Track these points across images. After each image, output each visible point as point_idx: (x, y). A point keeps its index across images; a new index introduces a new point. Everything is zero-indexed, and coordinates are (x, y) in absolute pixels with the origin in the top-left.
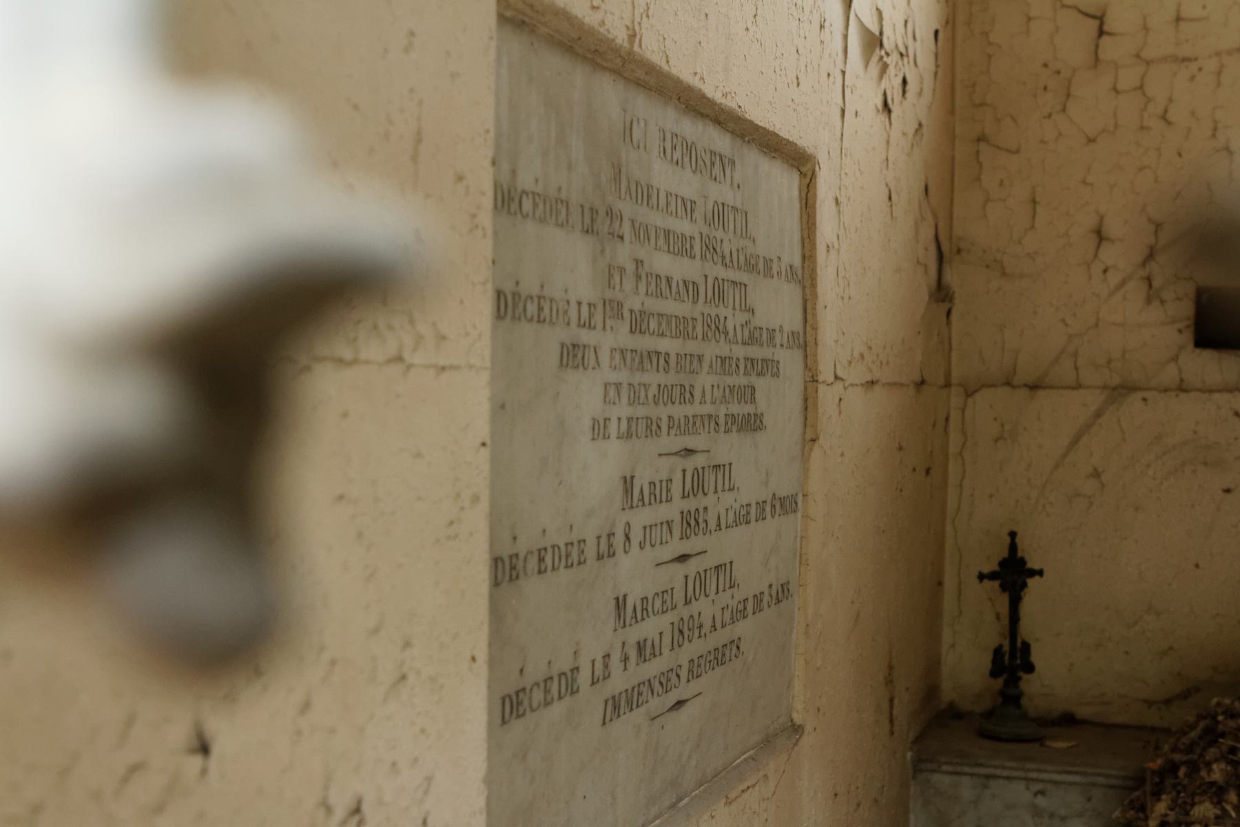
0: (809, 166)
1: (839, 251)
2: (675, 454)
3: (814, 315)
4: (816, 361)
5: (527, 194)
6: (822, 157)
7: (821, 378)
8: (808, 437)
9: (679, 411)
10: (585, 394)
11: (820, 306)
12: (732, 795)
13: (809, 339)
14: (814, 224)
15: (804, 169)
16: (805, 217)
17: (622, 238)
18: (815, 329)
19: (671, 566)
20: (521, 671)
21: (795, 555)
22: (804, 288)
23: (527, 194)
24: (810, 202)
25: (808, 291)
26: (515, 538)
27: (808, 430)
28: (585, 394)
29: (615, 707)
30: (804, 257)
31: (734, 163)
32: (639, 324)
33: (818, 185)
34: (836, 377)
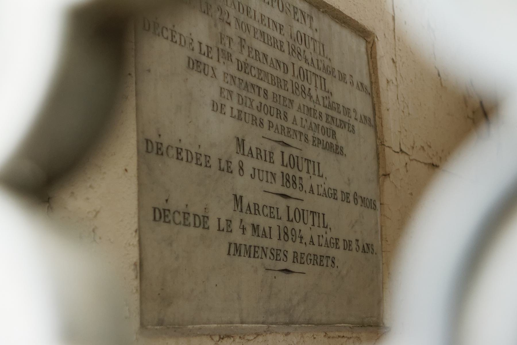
0: (371, 38)
1: (397, 86)
2: (276, 141)
3: (380, 112)
4: (382, 135)
5: (179, 213)
6: (379, 34)
7: (387, 144)
8: (381, 172)
9: (276, 121)
10: (208, 89)
11: (383, 108)
12: (331, 334)
13: (378, 123)
14: (376, 66)
15: (369, 40)
16: (371, 64)
17: (229, 24)
18: (381, 118)
19: (275, 195)
20: (167, 200)
21: (377, 232)
22: (373, 98)
23: (179, 213)
24: (373, 55)
25: (375, 100)
26: (160, 135)
27: (381, 170)
28: (208, 89)
29: (236, 249)
30: (371, 83)
31: (311, 18)
32: (243, 67)
33: (377, 48)
34: (401, 150)
